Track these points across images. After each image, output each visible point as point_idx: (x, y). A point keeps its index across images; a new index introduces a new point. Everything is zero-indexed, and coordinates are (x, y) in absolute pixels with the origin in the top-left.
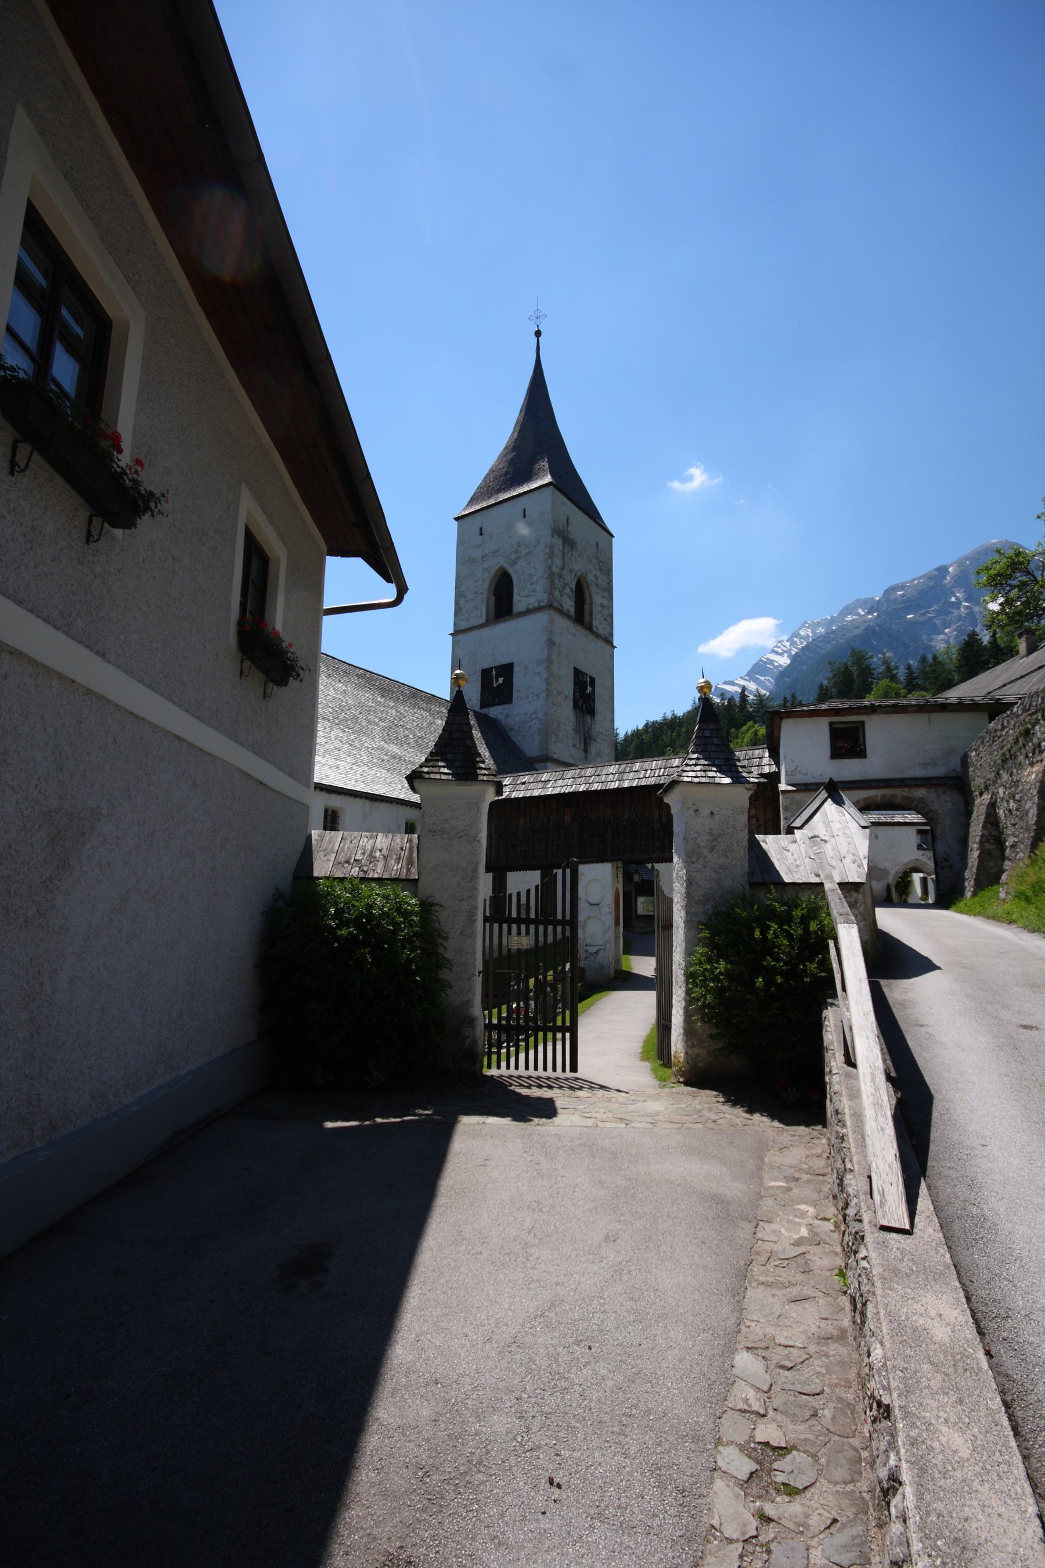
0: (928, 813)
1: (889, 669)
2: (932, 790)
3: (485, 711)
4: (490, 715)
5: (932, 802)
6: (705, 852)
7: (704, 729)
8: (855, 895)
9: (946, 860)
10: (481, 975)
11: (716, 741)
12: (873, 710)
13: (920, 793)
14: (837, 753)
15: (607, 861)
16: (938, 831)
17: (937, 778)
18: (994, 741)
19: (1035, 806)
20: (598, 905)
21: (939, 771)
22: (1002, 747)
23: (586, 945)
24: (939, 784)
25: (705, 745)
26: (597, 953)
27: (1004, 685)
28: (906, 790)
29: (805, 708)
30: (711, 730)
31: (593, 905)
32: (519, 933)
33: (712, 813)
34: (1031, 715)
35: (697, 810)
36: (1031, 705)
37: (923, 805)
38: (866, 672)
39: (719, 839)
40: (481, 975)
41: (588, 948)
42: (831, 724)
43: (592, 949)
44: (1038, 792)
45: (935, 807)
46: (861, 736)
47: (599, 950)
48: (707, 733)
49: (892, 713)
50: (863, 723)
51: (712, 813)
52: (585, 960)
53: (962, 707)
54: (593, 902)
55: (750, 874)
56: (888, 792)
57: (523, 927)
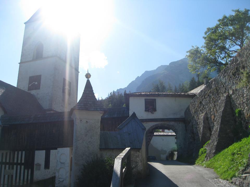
3: (30, 91)
4: (31, 93)
5: (176, 126)
8: (138, 153)
12: (158, 95)
13: (172, 123)
14: (147, 110)
15: (68, 147)
17: (178, 119)
20: (64, 163)
21: (178, 116)
22: (194, 108)
23: (59, 178)
26: (63, 181)
28: (168, 122)
31: (62, 163)
32: (9, 169)
33: (87, 122)
35: (81, 120)
36: (201, 94)
41: (59, 179)
42: (145, 99)
43: (61, 180)
47: (64, 180)
50: (155, 100)
51: (87, 122)
52: (58, 184)
54: (62, 162)
55: (100, 145)
56: (163, 123)
57: (11, 166)
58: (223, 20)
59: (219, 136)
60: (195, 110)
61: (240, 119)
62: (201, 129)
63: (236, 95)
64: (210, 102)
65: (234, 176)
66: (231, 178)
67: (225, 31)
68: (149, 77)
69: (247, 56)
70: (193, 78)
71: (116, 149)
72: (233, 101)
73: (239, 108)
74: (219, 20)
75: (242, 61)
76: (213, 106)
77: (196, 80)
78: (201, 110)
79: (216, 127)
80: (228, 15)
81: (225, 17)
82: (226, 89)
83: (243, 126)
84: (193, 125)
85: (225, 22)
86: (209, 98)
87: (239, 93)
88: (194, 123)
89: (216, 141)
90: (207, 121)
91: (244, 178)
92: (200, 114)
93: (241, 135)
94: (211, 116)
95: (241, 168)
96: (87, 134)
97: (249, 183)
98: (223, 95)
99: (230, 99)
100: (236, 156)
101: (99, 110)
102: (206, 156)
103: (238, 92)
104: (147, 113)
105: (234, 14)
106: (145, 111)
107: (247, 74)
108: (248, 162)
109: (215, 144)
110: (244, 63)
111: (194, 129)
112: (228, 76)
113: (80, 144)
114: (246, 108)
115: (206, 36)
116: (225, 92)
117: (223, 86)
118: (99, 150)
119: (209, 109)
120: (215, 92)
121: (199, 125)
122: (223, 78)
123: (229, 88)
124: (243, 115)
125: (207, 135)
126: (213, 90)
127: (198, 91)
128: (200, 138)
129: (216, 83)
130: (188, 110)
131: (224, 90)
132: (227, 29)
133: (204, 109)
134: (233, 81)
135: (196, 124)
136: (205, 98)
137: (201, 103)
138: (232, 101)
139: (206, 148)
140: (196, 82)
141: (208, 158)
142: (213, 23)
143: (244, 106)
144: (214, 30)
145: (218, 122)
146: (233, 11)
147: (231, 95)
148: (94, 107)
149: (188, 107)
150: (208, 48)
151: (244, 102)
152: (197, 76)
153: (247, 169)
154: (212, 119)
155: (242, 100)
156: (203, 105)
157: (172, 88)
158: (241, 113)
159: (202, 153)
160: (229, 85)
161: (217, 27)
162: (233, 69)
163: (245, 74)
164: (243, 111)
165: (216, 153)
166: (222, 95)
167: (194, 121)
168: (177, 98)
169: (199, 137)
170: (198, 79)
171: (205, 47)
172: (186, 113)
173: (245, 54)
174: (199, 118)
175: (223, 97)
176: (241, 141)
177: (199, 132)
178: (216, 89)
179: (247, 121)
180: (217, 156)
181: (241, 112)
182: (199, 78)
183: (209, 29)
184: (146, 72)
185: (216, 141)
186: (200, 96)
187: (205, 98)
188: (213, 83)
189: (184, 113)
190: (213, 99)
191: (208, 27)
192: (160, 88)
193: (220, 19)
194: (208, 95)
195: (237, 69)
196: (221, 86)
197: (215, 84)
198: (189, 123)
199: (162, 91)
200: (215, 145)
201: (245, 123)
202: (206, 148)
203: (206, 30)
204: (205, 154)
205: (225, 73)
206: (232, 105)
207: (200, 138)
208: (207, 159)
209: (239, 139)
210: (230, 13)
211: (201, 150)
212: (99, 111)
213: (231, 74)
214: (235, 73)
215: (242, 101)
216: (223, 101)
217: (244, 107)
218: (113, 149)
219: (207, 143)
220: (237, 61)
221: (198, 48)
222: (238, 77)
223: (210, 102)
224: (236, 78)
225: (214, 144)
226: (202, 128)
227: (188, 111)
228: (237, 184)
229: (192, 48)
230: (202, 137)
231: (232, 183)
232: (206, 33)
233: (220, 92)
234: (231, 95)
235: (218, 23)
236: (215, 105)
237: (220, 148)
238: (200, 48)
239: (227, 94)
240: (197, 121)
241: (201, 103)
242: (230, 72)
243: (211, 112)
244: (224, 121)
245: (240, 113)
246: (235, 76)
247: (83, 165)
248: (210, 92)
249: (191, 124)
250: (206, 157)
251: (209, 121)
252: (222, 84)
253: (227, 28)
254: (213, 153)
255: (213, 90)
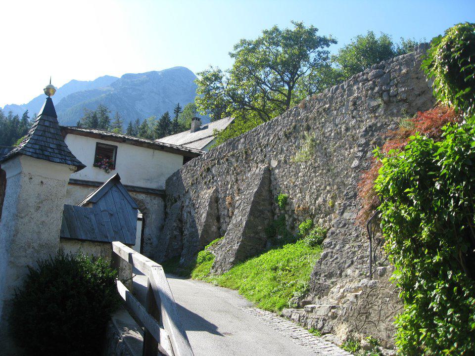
0: (144, 210)
1: (118, 123)
2: (149, 196)
6: (33, 210)
7: (45, 120)
9: (150, 239)
10: (202, 215)
11: (52, 131)
12: (123, 140)
13: (141, 197)
16: (148, 221)
17: (152, 190)
18: (188, 172)
19: (206, 212)
22: (193, 176)
24: (152, 193)
25: (44, 131)
27: (191, 142)
28: (135, 193)
29: (84, 130)
30: (50, 122)
33: (42, 182)
34: (212, 160)
36: (212, 155)
37: (142, 204)
38: (106, 120)
39: (44, 203)
40: (202, 215)
44: (209, 205)
45: (149, 206)
46: (114, 155)
48: (47, 123)
49: (134, 145)
50: (116, 147)
51: (42, 182)
53: (172, 150)
55: (62, 231)
58: (271, 33)
59: (244, 234)
60: (193, 180)
61: (282, 212)
62: (203, 217)
63: (284, 171)
64: (228, 172)
65: (285, 306)
66: (280, 309)
67: (270, 52)
68: (77, 93)
69: (318, 111)
70: (167, 114)
71: (100, 242)
72: (276, 179)
73: (284, 192)
74: (265, 32)
75: (307, 117)
76: (232, 181)
77: (172, 119)
78: (205, 183)
79: (239, 218)
80: (282, 28)
81: (276, 29)
82: (265, 156)
83: (287, 223)
84: (183, 207)
85: (273, 36)
86: (228, 165)
87: (290, 168)
88: (187, 203)
89: (238, 243)
90: (216, 205)
91: (310, 310)
92: (202, 189)
93: (279, 237)
94: (225, 197)
95: (297, 294)
96: (40, 207)
97: (318, 319)
98: (258, 166)
99: (270, 175)
100: (280, 272)
101: (70, 162)
102: (214, 266)
103: (288, 166)
104: (97, 170)
105: (293, 28)
106: (95, 165)
107: (313, 140)
108: (309, 286)
109: (236, 247)
110: (310, 122)
111: (185, 214)
112: (275, 135)
113: (24, 225)
114: (298, 196)
115: (234, 52)
116: (263, 161)
117: (262, 150)
118: (59, 240)
119: (224, 184)
120: (242, 157)
121: (198, 208)
122: (263, 137)
123: (273, 157)
124: (289, 206)
125: (212, 229)
126: (239, 153)
127: (177, 140)
128: (200, 232)
129: (247, 142)
130: (175, 178)
131: (260, 158)
132: (274, 51)
133: (213, 182)
134: (282, 147)
135: (190, 205)
136: (219, 163)
137: (208, 169)
138: (272, 179)
139: (211, 251)
140: (171, 123)
141: (219, 271)
142: (254, 35)
143: (295, 191)
144: (250, 48)
145: (243, 210)
146: (293, 23)
147: (272, 169)
148: (59, 156)
149: (177, 172)
150: (236, 76)
151: (296, 186)
152: (175, 111)
153: (308, 296)
154: (227, 203)
155: (293, 180)
156: (213, 175)
157: (120, 125)
158: (288, 201)
159: (204, 259)
160: (274, 152)
161: (259, 43)
162: (286, 126)
163: (309, 141)
164: (292, 199)
165: (234, 264)
166: (254, 165)
167: (188, 201)
168: (157, 152)
169: (197, 230)
170: (177, 117)
171: (232, 72)
172: (169, 181)
173: (316, 108)
174: (198, 196)
175: (258, 170)
176: (282, 248)
177: (197, 221)
178: (246, 152)
179: (296, 217)
180: (239, 269)
181: (288, 200)
182: (177, 115)
183: (243, 42)
184: (74, 82)
185: (238, 243)
186: (208, 157)
187: (219, 163)
188: (242, 140)
189: (165, 182)
190: (235, 169)
191: (243, 38)
192: (99, 121)
193: (268, 31)
194: (227, 160)
195: (295, 127)
196: (257, 149)
197: (244, 143)
198: (176, 201)
199: (103, 128)
200: (235, 250)
201: (291, 219)
202: (211, 251)
203: (238, 42)
204: (212, 263)
205: (269, 129)
206: (272, 185)
207: (200, 232)
208: (216, 271)
209: (278, 244)
210: (286, 25)
211: (201, 254)
212: (69, 165)
213: (281, 133)
214: (290, 133)
215: (294, 183)
216: (257, 175)
217: (294, 192)
218: (83, 241)
219: (213, 242)
220: (299, 114)
221: (220, 71)
222: (293, 141)
223: (228, 172)
224: (289, 143)
225: (232, 247)
226: (204, 215)
227: (174, 180)
228: (293, 319)
229: (208, 69)
230: (204, 231)
231: (282, 316)
232: (236, 47)
233: (253, 159)
234: (273, 169)
235: (262, 35)
236: (237, 180)
237: (244, 255)
238: (224, 73)
239: (266, 166)
240: (193, 201)
241: (208, 169)
242: (281, 129)
243: (227, 189)
244: (256, 211)
245: (286, 201)
246: (288, 139)
247: (28, 266)
248: (233, 155)
249: (179, 203)
250: (213, 267)
251: (219, 205)
252: (261, 147)
253: (274, 49)
254: (230, 263)
255: (239, 153)
